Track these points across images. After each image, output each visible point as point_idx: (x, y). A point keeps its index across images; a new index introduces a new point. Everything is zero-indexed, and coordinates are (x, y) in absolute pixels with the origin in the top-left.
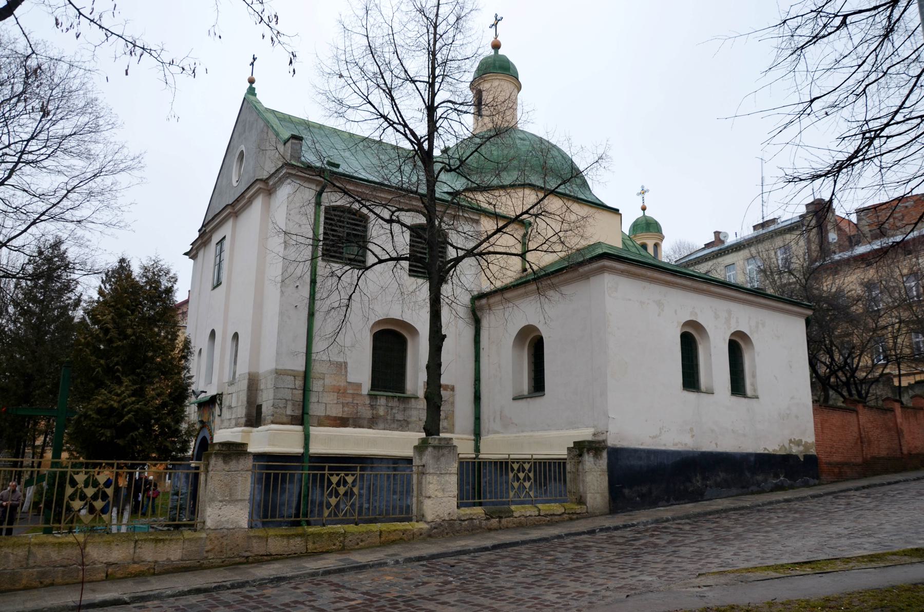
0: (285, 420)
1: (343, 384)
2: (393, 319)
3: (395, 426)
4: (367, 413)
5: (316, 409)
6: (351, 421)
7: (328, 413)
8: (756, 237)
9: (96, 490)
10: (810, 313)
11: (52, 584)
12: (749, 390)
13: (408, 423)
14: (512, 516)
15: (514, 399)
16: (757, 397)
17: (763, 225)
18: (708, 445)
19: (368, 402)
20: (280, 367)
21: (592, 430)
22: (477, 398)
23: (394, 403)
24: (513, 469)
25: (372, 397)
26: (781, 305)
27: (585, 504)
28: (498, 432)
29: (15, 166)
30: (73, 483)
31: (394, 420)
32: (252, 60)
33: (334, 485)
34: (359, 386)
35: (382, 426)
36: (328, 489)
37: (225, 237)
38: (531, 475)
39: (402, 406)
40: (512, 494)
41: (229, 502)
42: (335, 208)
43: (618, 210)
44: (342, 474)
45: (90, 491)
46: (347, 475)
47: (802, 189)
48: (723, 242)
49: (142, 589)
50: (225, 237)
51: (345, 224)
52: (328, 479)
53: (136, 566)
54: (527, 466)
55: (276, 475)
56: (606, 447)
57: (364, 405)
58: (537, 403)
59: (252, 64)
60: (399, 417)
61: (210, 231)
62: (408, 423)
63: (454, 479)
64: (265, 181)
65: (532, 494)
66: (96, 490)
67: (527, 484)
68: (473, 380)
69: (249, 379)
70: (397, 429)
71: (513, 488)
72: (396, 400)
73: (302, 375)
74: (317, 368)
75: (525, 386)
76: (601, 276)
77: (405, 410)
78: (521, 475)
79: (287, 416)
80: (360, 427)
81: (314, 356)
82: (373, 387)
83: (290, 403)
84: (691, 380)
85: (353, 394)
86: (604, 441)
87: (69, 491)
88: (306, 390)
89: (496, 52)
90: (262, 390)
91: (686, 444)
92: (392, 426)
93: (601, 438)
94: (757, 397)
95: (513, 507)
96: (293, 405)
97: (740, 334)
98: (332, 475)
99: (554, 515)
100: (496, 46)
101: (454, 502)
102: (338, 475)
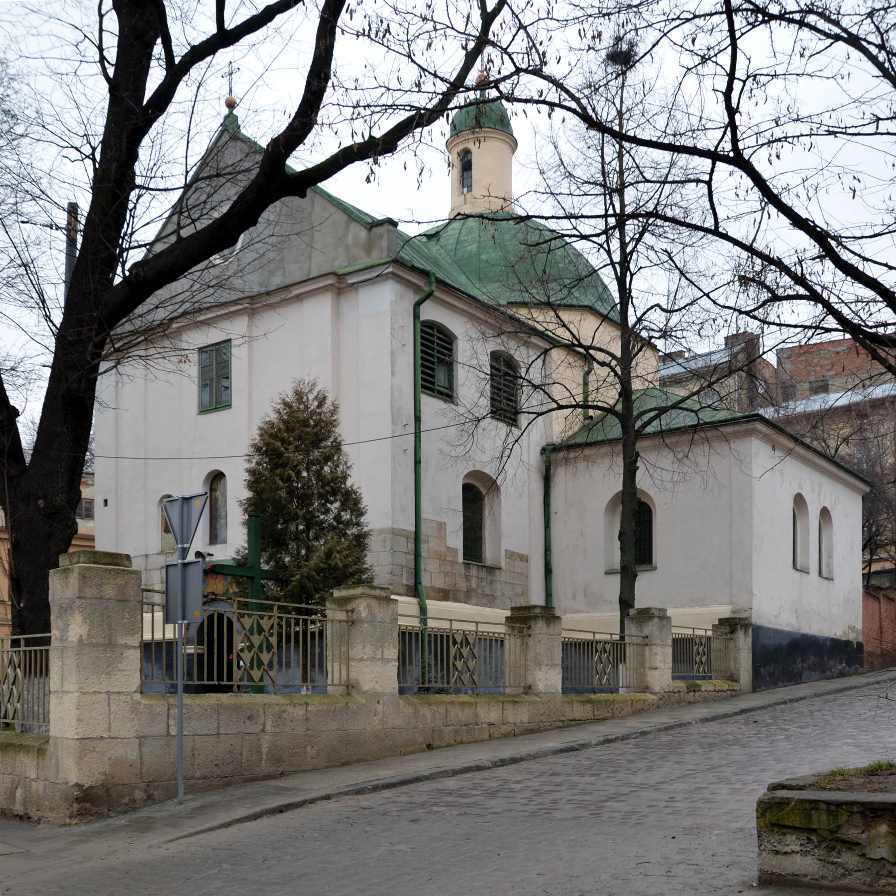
1: (443, 549)
3: (484, 601)
4: (462, 585)
5: (426, 581)
7: (433, 584)
10: (868, 489)
11: (462, 743)
13: (494, 598)
15: (606, 573)
20: (395, 526)
21: (730, 607)
22: (548, 571)
25: (467, 566)
28: (582, 612)
34: (455, 551)
35: (474, 601)
49: (508, 750)
51: (435, 346)
53: (504, 727)
56: (751, 625)
60: (488, 591)
62: (494, 598)
64: (340, 277)
68: (543, 550)
72: (485, 570)
74: (425, 529)
76: (748, 439)
81: (424, 516)
83: (404, 569)
86: (746, 619)
87: (453, 650)
93: (743, 616)
101: (670, 675)
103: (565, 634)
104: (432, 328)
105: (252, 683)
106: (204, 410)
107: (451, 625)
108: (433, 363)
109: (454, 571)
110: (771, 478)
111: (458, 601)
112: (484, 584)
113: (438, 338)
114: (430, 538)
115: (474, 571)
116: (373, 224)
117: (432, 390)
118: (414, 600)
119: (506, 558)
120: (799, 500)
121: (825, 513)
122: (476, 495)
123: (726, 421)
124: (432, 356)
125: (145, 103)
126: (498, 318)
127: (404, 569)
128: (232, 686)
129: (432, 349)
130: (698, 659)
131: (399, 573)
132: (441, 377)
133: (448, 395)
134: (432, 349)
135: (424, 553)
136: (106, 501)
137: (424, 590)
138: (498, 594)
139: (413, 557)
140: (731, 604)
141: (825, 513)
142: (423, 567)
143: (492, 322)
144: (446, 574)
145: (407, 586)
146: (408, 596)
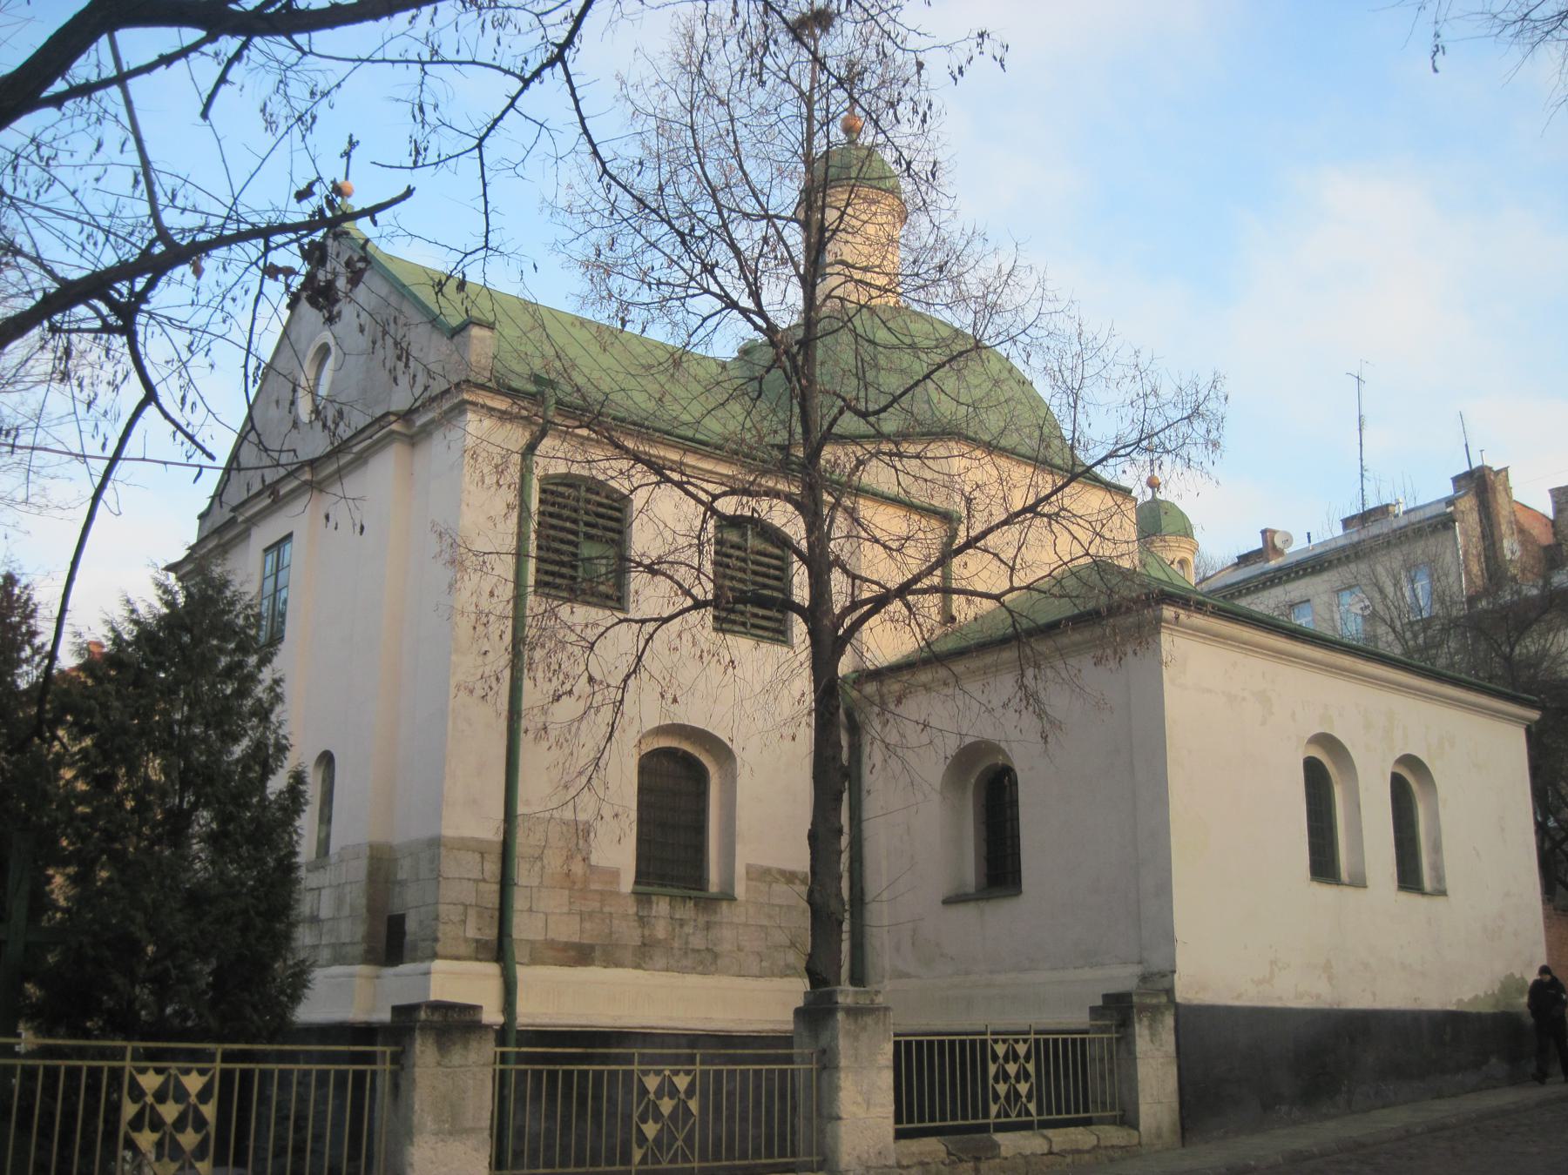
0: (463, 950)
2: (693, 728)
3: (688, 962)
5: (524, 928)
6: (597, 953)
7: (551, 935)
8: (1354, 546)
9: (181, 1107)
10: (1535, 715)
12: (1427, 883)
13: (716, 956)
14: (997, 1156)
16: (1443, 893)
17: (1365, 518)
18: (1359, 998)
19: (632, 910)
21: (1137, 970)
23: (687, 911)
24: (995, 1058)
25: (642, 898)
27: (1134, 1125)
30: (137, 1093)
31: (687, 951)
32: (345, 146)
33: (652, 1096)
34: (615, 874)
35: (661, 961)
36: (639, 1104)
37: (289, 537)
38: (1031, 1067)
39: (702, 919)
40: (994, 1109)
41: (451, 1134)
42: (568, 481)
44: (173, 1066)
45: (170, 1111)
46: (676, 1073)
47: (167, 60)
48: (1278, 552)
50: (289, 537)
52: (640, 1080)
54: (1021, 1049)
55: (341, 1076)
57: (625, 916)
58: (1001, 914)
59: (347, 154)
60: (697, 942)
61: (248, 520)
62: (716, 956)
63: (887, 1078)
65: (1032, 1107)
66: (181, 1107)
67: (1023, 1088)
69: (372, 858)
70: (692, 970)
71: (996, 1097)
72: (691, 904)
73: (498, 849)
74: (524, 842)
75: (970, 873)
77: (708, 926)
78: (1012, 1068)
79: (466, 940)
80: (616, 965)
81: (521, 809)
82: (641, 877)
83: (472, 912)
84: (1324, 865)
85: (602, 893)
87: (129, 1110)
88: (506, 883)
90: (402, 883)
91: (1318, 996)
92: (684, 962)
94: (1443, 893)
95: (999, 1137)
96: (480, 916)
97: (1411, 762)
98: (645, 1073)
99: (1078, 1151)
101: (889, 1126)
102: (658, 1073)
109: (607, 909)
111: (618, 964)
112: (688, 929)
119: (749, 878)
123: (1257, 589)
125: (45, 94)
127: (472, 912)
128: (702, 1063)
130: (1002, 1088)
138: (726, 947)
139: (496, 887)
140: (1140, 963)
143: (503, 407)
145: (477, 941)
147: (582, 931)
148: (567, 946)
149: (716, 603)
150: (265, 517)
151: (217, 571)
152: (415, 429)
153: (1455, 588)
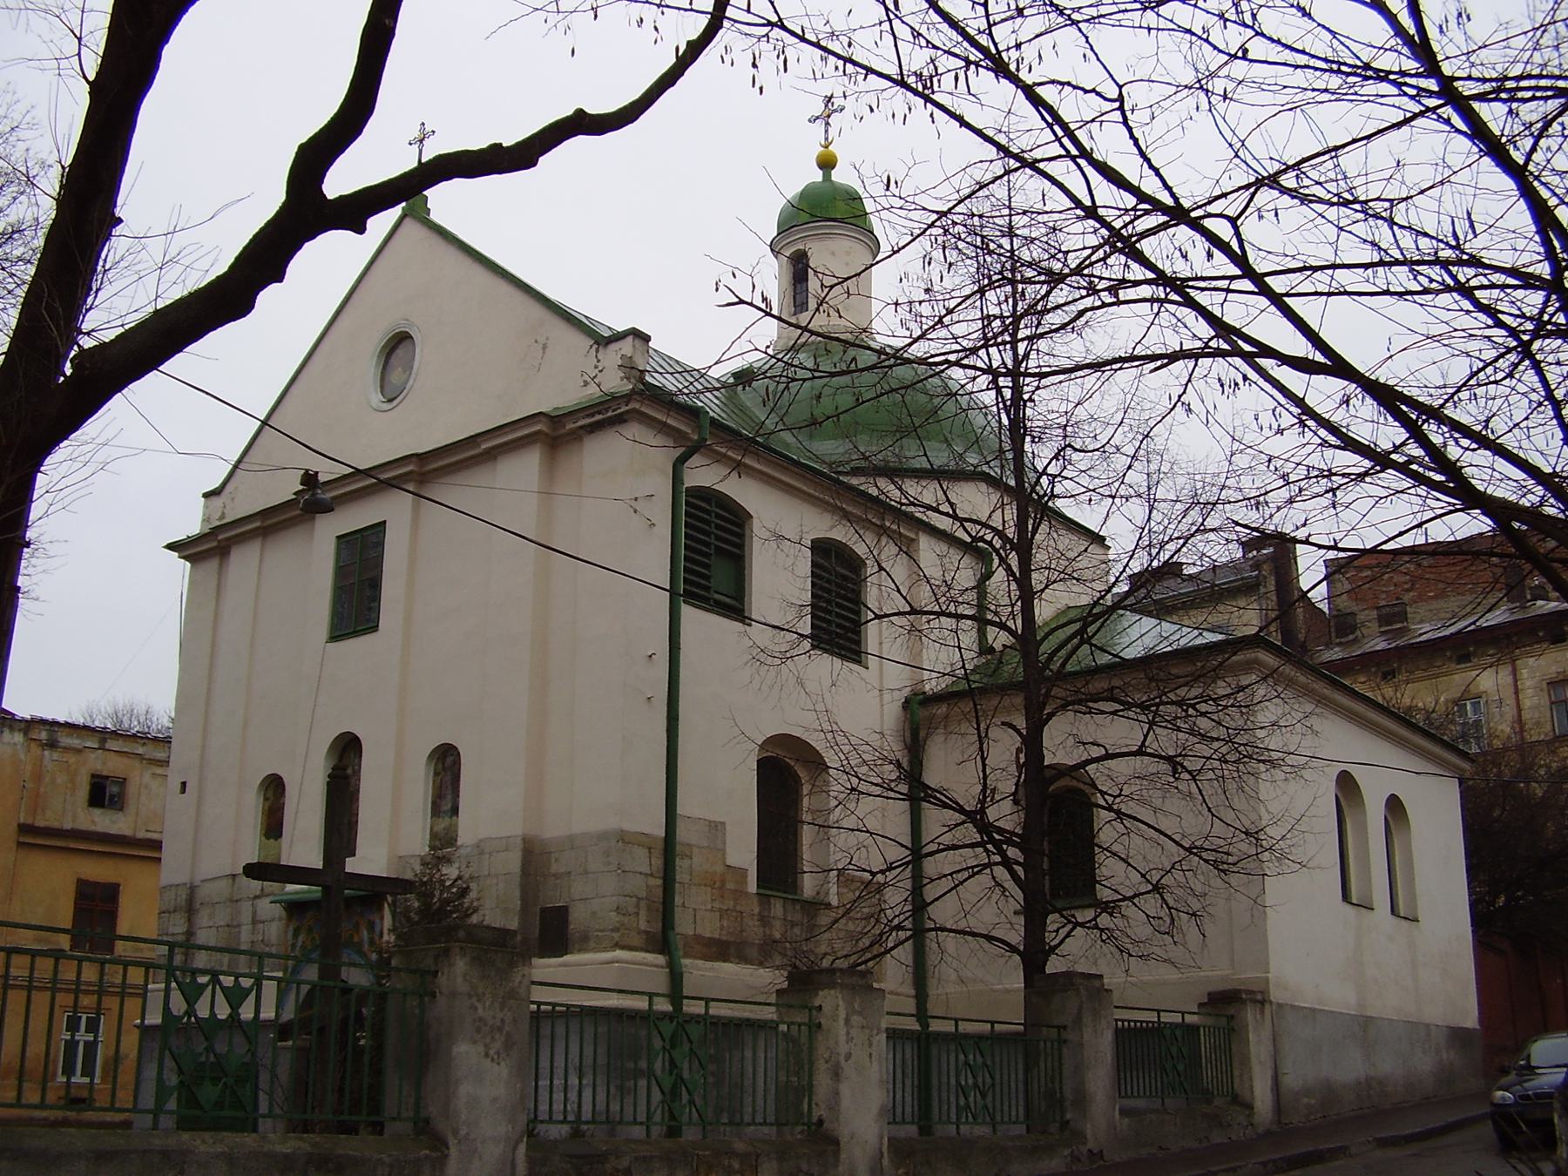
1: (719, 868)
4: (754, 931)
5: (684, 925)
7: (699, 931)
26: (1437, 750)
29: (1397, 263)
43: (1103, 539)
47: (1401, 534)
73: (661, 845)
74: (683, 833)
81: (682, 809)
82: (762, 880)
83: (643, 904)
89: (827, 177)
96: (649, 908)
100: (827, 164)
103: (1119, 1014)
104: (708, 501)
105: (198, 1112)
106: (336, 636)
107: (650, 1004)
108: (707, 555)
110: (1311, 754)
113: (718, 516)
114: (695, 850)
115: (777, 908)
116: (604, 340)
117: (706, 600)
118: (660, 959)
120: (1346, 783)
121: (1395, 806)
122: (784, 773)
124: (707, 544)
126: (825, 486)
129: (708, 534)
131: (632, 910)
132: (720, 575)
133: (735, 607)
134: (708, 534)
135: (681, 875)
136: (184, 784)
137: (680, 944)
141: (1395, 806)
142: (678, 900)
144: (723, 913)
145: (647, 933)
146: (647, 951)
147: (722, 928)
148: (711, 942)
149: (812, 636)
150: (467, 467)
151: (731, 380)
152: (562, 431)
153: (1126, 640)
